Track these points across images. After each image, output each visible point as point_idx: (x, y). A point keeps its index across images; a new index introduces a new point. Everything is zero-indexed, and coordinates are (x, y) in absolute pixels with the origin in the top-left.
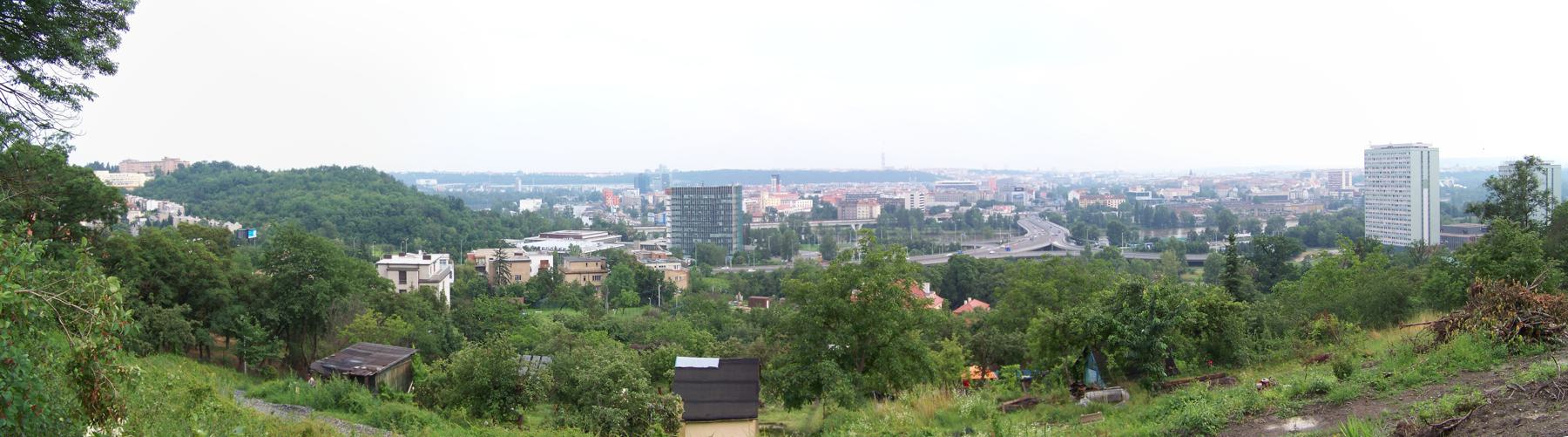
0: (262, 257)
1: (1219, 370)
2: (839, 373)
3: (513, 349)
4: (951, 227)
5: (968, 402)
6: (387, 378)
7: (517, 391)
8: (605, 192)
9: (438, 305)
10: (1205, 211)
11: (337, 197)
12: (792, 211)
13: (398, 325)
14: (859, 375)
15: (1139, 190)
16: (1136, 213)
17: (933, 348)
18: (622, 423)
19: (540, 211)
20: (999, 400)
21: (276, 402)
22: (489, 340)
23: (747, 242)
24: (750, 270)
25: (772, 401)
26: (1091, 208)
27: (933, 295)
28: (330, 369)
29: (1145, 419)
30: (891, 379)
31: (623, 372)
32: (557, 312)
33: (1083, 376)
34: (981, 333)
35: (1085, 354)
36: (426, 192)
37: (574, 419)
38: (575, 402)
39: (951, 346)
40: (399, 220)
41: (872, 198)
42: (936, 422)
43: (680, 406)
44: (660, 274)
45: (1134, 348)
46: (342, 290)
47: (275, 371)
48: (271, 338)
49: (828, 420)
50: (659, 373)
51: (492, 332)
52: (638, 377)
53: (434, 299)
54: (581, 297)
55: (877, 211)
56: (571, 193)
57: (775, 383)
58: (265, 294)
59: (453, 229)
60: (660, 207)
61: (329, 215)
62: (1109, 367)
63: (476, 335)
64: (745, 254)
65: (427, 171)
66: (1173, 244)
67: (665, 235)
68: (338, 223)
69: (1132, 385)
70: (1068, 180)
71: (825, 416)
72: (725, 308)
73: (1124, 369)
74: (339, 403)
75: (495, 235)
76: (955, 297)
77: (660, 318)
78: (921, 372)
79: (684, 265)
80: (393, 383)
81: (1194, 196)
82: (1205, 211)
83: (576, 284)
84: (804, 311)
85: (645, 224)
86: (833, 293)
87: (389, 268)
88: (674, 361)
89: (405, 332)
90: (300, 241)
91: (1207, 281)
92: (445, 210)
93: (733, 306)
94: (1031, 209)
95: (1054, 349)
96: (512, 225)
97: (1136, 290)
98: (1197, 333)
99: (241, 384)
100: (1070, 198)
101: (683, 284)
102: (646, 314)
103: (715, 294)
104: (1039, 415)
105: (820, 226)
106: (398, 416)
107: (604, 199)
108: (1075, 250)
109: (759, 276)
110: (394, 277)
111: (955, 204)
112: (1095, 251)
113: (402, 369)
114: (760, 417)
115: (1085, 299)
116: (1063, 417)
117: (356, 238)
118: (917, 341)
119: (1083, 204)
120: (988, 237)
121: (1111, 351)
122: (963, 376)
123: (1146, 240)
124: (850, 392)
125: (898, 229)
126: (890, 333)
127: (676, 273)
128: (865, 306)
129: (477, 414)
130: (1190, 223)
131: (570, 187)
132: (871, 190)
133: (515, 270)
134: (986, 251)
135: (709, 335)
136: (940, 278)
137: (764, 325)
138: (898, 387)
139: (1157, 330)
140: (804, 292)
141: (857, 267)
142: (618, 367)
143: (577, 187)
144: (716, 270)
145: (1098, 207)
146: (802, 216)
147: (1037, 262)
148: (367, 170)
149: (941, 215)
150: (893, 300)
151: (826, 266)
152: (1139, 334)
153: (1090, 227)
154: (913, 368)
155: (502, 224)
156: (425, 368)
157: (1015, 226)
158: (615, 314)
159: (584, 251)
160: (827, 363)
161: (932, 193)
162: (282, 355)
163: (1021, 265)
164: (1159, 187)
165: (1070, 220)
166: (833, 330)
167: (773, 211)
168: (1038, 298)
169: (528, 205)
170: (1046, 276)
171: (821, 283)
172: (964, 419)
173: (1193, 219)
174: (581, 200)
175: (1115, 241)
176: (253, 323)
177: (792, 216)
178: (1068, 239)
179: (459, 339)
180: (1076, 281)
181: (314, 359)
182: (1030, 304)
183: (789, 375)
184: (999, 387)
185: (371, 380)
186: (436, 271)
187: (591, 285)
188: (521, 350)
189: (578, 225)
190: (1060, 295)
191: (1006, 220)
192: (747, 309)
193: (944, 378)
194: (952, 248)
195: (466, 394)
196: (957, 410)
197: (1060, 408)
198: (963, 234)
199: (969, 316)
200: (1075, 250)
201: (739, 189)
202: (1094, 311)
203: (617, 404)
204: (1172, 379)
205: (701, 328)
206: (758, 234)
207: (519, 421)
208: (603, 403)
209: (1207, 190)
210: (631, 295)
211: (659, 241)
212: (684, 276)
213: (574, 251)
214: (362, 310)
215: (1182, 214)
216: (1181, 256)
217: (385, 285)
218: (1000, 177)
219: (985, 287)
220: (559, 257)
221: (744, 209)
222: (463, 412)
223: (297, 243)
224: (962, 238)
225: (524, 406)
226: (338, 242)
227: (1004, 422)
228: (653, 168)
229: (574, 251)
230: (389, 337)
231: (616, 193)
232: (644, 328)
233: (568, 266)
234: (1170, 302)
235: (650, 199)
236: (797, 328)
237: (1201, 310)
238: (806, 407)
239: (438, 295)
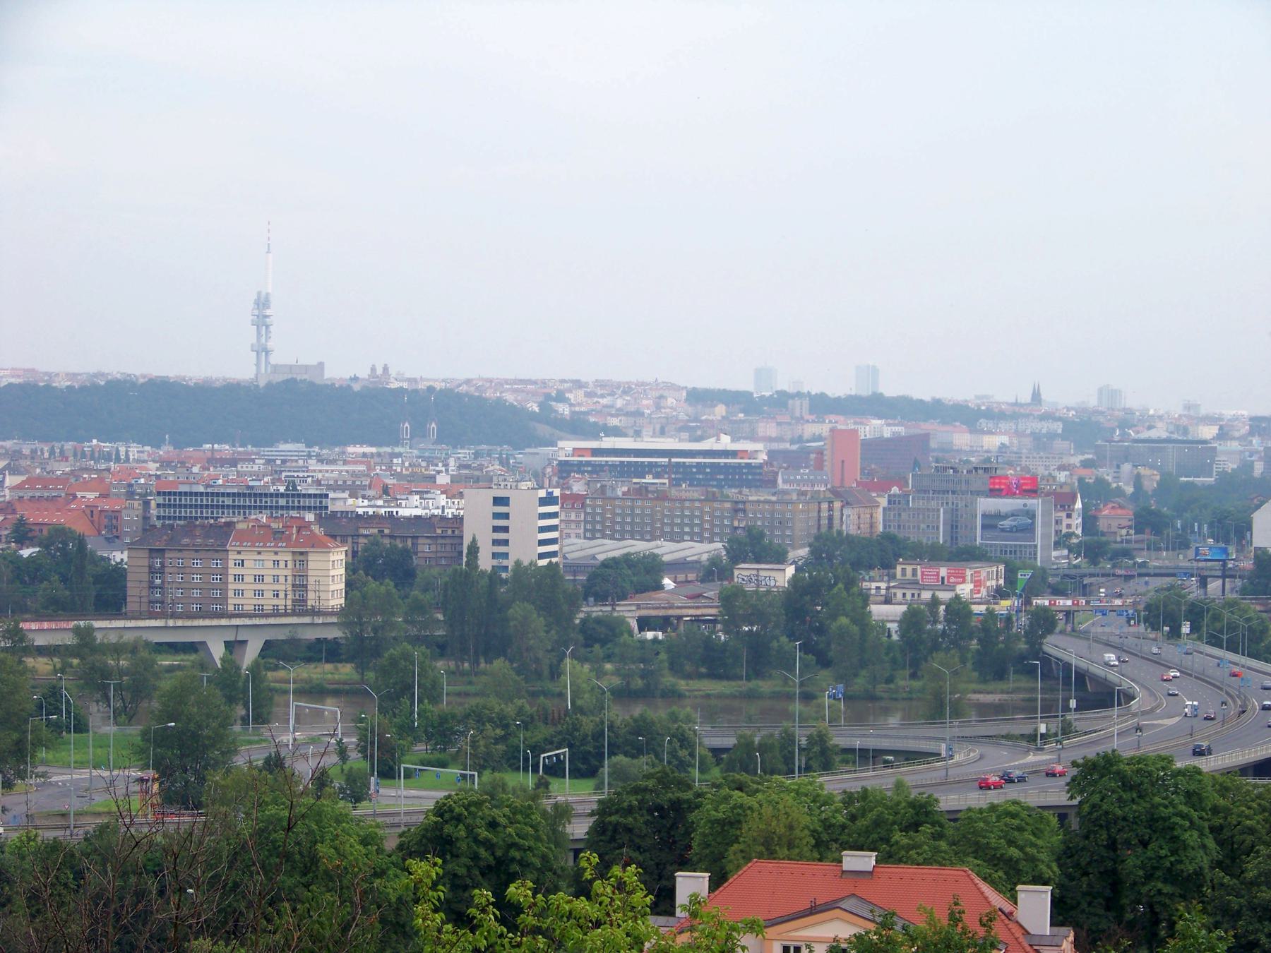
41: (295, 516)
55: (330, 574)
90: (403, 926)
111: (701, 550)
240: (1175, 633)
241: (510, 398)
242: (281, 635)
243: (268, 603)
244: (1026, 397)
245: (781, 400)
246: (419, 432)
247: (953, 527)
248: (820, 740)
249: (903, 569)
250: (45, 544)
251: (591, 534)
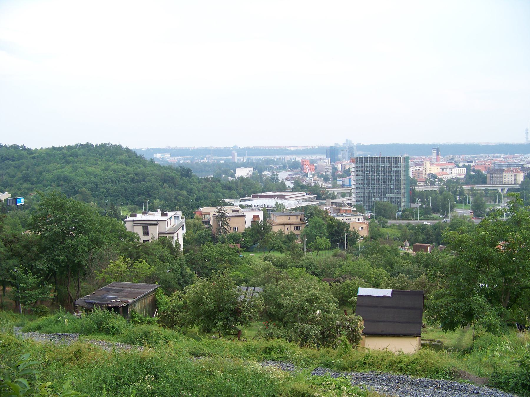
0: (30, 219)
2: (488, 306)
3: (233, 283)
6: (137, 307)
7: (236, 313)
8: (303, 161)
9: (174, 251)
11: (91, 169)
12: (449, 177)
13: (144, 267)
14: (504, 309)
18: (316, 336)
19: (252, 177)
21: (49, 332)
22: (214, 276)
23: (413, 201)
25: (433, 324)
28: (92, 304)
31: (317, 299)
32: (266, 254)
36: (162, 164)
37: (280, 332)
38: (281, 320)
40: (142, 186)
41: (516, 167)
43: (361, 324)
44: (346, 225)
46: (98, 243)
47: (47, 309)
48: (42, 283)
50: (345, 300)
51: (216, 270)
53: (170, 246)
54: (285, 243)
55: (521, 178)
56: (273, 162)
57: (436, 310)
58: (35, 249)
59: (184, 192)
60: (347, 173)
61: (85, 184)
63: (204, 272)
64: (411, 210)
65: (163, 146)
68: (92, 190)
71: (475, 338)
74: (101, 329)
75: (217, 196)
77: (346, 258)
79: (365, 218)
80: (141, 311)
83: (281, 233)
85: (335, 186)
86: (484, 244)
87: (135, 224)
89: (149, 273)
92: (178, 177)
93: (401, 251)
96: (230, 189)
99: (18, 321)
101: (364, 233)
102: (336, 255)
103: (390, 241)
105: (472, 189)
106: (147, 334)
107: (303, 167)
110: (139, 230)
113: (148, 300)
114: (422, 335)
117: (106, 202)
124: (496, 321)
127: (359, 224)
129: (207, 330)
131: (275, 158)
132: (516, 160)
133: (233, 223)
135: (385, 272)
140: (461, 242)
142: (313, 295)
143: (281, 157)
144: (390, 222)
146: (457, 181)
148: (114, 146)
151: (477, 221)
155: (223, 187)
156: (166, 299)
158: (311, 255)
160: (478, 297)
162: (51, 296)
166: (484, 272)
167: (434, 176)
169: (242, 172)
174: (284, 168)
176: (26, 273)
177: (449, 181)
179: (191, 276)
181: (78, 297)
183: (447, 305)
185: (125, 309)
186: (173, 224)
187: (292, 234)
188: (239, 283)
189: (282, 188)
192: (413, 253)
195: (198, 316)
201: (406, 159)
203: (312, 321)
205: (378, 266)
206: (422, 195)
207: (239, 334)
208: (302, 321)
210: (324, 241)
211: (345, 200)
212: (365, 226)
213: (279, 208)
214: (115, 257)
217: (132, 237)
220: (267, 212)
221: (411, 175)
222: (196, 329)
223: (60, 207)
225: (242, 323)
226: (93, 205)
229: (279, 208)
230: (137, 277)
231: (312, 162)
232: (334, 266)
233: (274, 219)
235: (339, 167)
238: (459, 329)
239: (174, 244)
243: (510, 182)
250: (476, 173)
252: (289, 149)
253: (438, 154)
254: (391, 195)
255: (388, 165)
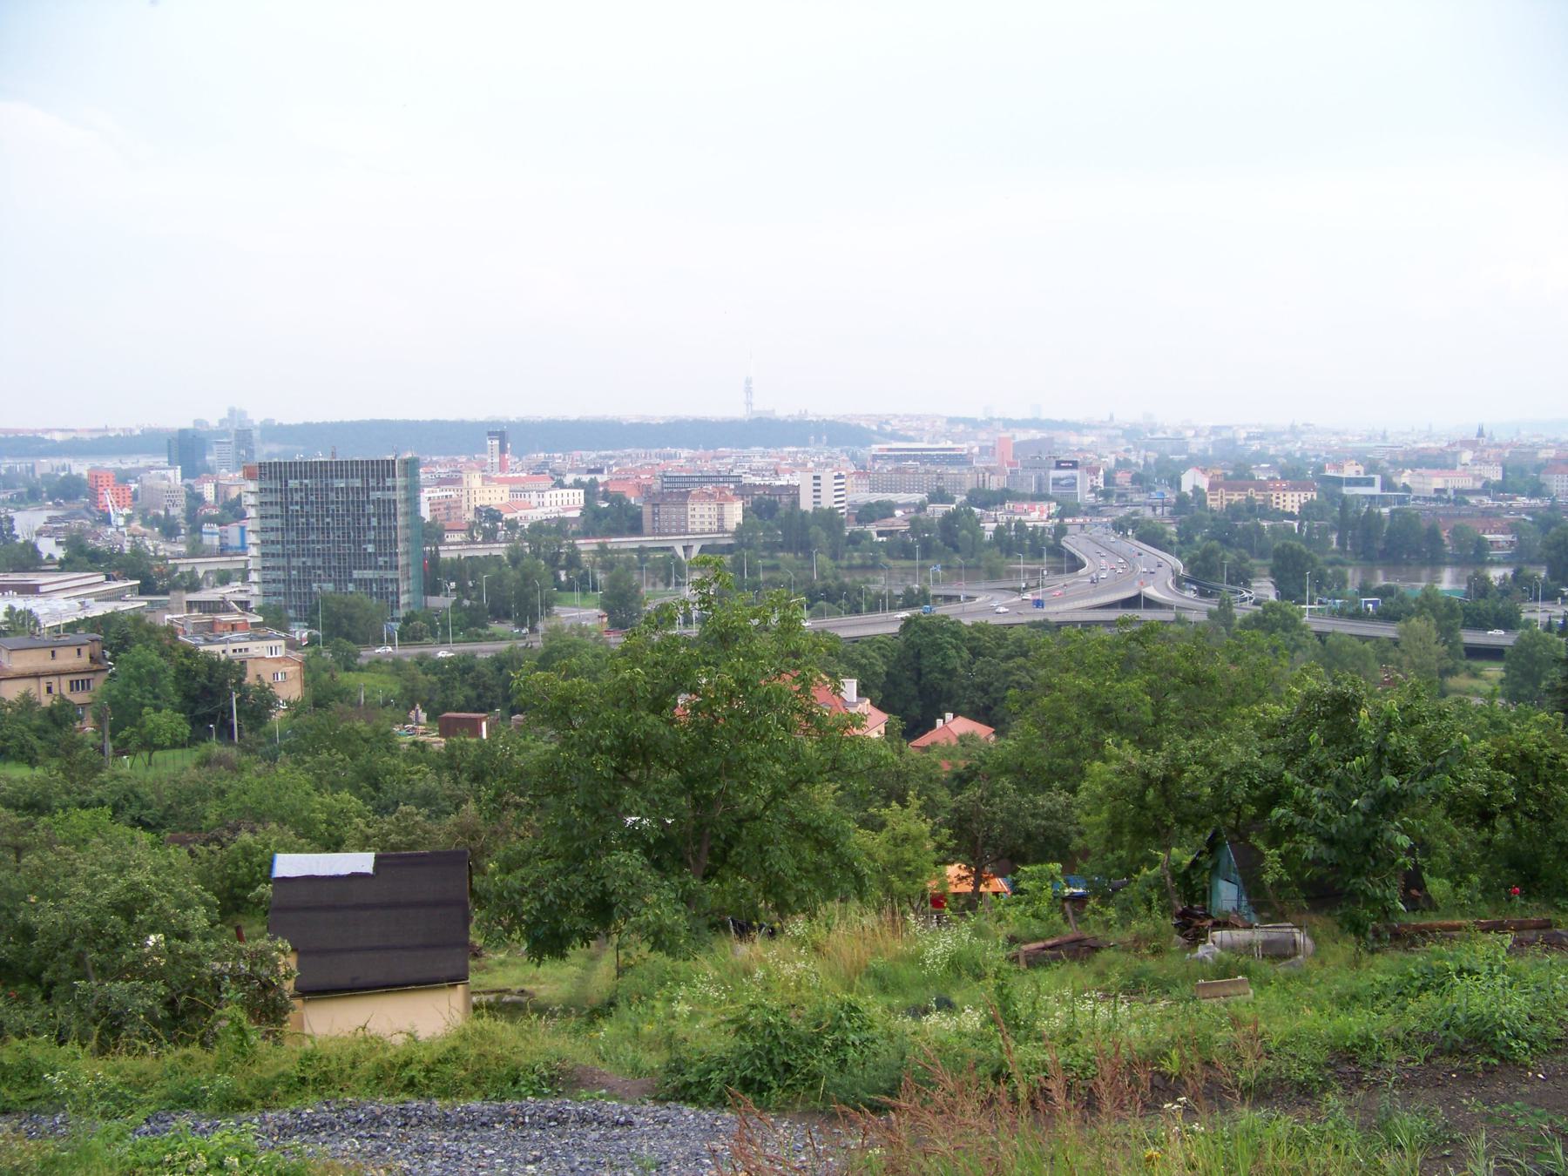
1: (1535, 912)
2: (651, 878)
4: (907, 552)
5: (941, 943)
10: (1513, 528)
12: (537, 515)
14: (695, 883)
15: (1350, 471)
16: (1343, 525)
17: (864, 824)
18: (150, 1014)
20: (1013, 940)
23: (434, 589)
24: (443, 654)
25: (500, 943)
26: (1234, 511)
27: (865, 706)
29: (1347, 1001)
30: (767, 891)
31: (147, 899)
33: (1206, 894)
34: (973, 792)
35: (1213, 845)
38: (34, 978)
39: (905, 819)
41: (721, 485)
42: (869, 984)
44: (236, 669)
45: (1330, 841)
49: (629, 978)
50: (240, 894)
52: (186, 905)
54: (41, 733)
55: (735, 514)
57: (506, 904)
60: (234, 511)
62: (1269, 878)
64: (430, 616)
66: (1430, 604)
67: (244, 575)
69: (1320, 922)
70: (1180, 443)
71: (621, 971)
72: (386, 742)
73: (1303, 885)
76: (916, 711)
77: (236, 769)
78: (832, 875)
79: (292, 645)
81: (1487, 488)
82: (1513, 528)
83: (28, 703)
84: (567, 744)
85: (196, 550)
86: (633, 704)
88: (270, 865)
91: (1514, 697)
93: (403, 737)
94: (1094, 510)
95: (1140, 832)
97: (1344, 706)
98: (1485, 817)
100: (1186, 487)
101: (290, 689)
102: (206, 762)
103: (371, 709)
104: (1101, 975)
105: (603, 550)
107: (94, 494)
108: (1198, 609)
109: (463, 668)
111: (917, 497)
112: (1242, 611)
114: (473, 978)
115: (1216, 722)
116: (1157, 983)
118: (828, 808)
119: (1216, 502)
120: (993, 574)
121: (1274, 842)
122: (932, 885)
123: (1364, 590)
124: (676, 919)
125: (785, 556)
126: (765, 790)
127: (274, 663)
128: (707, 732)
130: (1475, 555)
132: (720, 467)
134: (989, 606)
135: (355, 803)
136: (881, 668)
137: (478, 777)
138: (783, 908)
139: (1388, 804)
140: (567, 701)
141: (689, 643)
142: (134, 887)
143: (20, 465)
145: (1252, 509)
146: (559, 527)
147: (1105, 633)
149: (884, 525)
150: (771, 718)
151: (617, 640)
152: (1347, 809)
153: (1230, 556)
154: (818, 868)
157: (1057, 551)
158: (129, 767)
159: (47, 623)
160: (622, 857)
161: (862, 472)
163: (1067, 641)
164: (1400, 464)
165: (1186, 537)
166: (636, 784)
167: (492, 515)
168: (1105, 716)
170: (1127, 666)
171: (607, 681)
172: (932, 978)
173: (1481, 547)
174: (32, 496)
175: (1290, 587)
177: (538, 528)
178: (1179, 582)
180: (1196, 680)
182: (1088, 730)
183: (537, 884)
184: (1013, 912)
187: (65, 703)
189: (29, 559)
190: (1157, 710)
191: (1035, 536)
192: (437, 742)
193: (889, 891)
194: (910, 601)
196: (916, 959)
197: (1152, 963)
198: (936, 569)
199: (948, 753)
200: (1198, 609)
201: (411, 466)
202: (1239, 749)
203: (134, 970)
204: (1414, 920)
205: (337, 787)
206: (458, 570)
208: (104, 972)
209: (1522, 474)
210: (166, 720)
211: (231, 592)
212: (293, 670)
215: (1456, 532)
216: (1447, 633)
218: (1021, 436)
219: (984, 689)
221: (426, 513)
224: (932, 578)
227: (1023, 988)
228: (212, 414)
231: (123, 478)
232: (201, 794)
234: (1424, 740)
235: (209, 492)
236: (552, 781)
237: (1498, 763)
240: (1125, 535)
241: (863, 424)
242: (708, 543)
243: (707, 527)
244: (1107, 418)
245: (990, 422)
246: (818, 440)
247: (1040, 485)
248: (923, 592)
249: (1009, 505)
251: (873, 489)
252: (47, 437)
253: (503, 450)
254: (369, 574)
255: (358, 483)
